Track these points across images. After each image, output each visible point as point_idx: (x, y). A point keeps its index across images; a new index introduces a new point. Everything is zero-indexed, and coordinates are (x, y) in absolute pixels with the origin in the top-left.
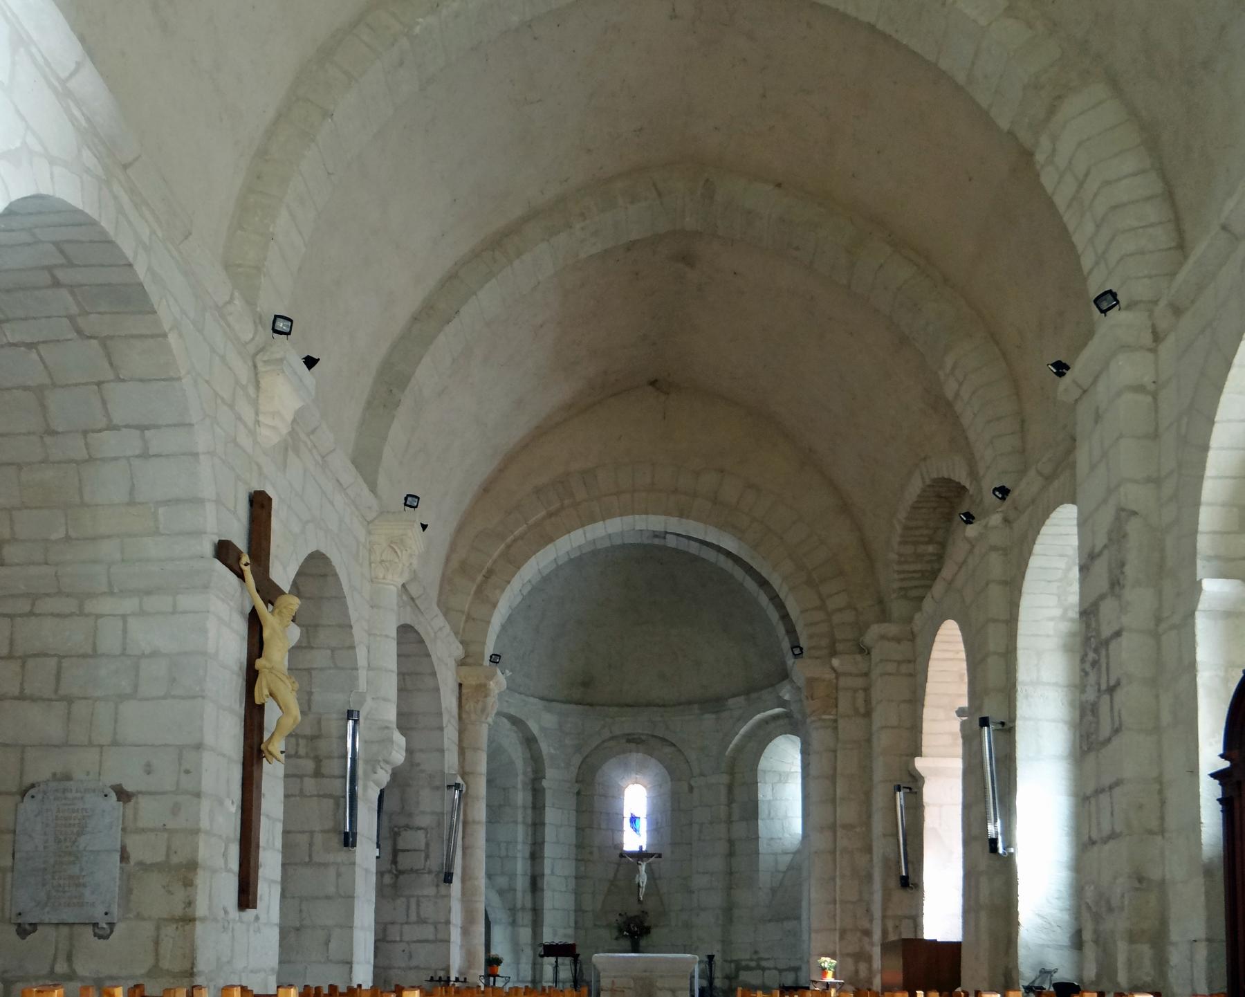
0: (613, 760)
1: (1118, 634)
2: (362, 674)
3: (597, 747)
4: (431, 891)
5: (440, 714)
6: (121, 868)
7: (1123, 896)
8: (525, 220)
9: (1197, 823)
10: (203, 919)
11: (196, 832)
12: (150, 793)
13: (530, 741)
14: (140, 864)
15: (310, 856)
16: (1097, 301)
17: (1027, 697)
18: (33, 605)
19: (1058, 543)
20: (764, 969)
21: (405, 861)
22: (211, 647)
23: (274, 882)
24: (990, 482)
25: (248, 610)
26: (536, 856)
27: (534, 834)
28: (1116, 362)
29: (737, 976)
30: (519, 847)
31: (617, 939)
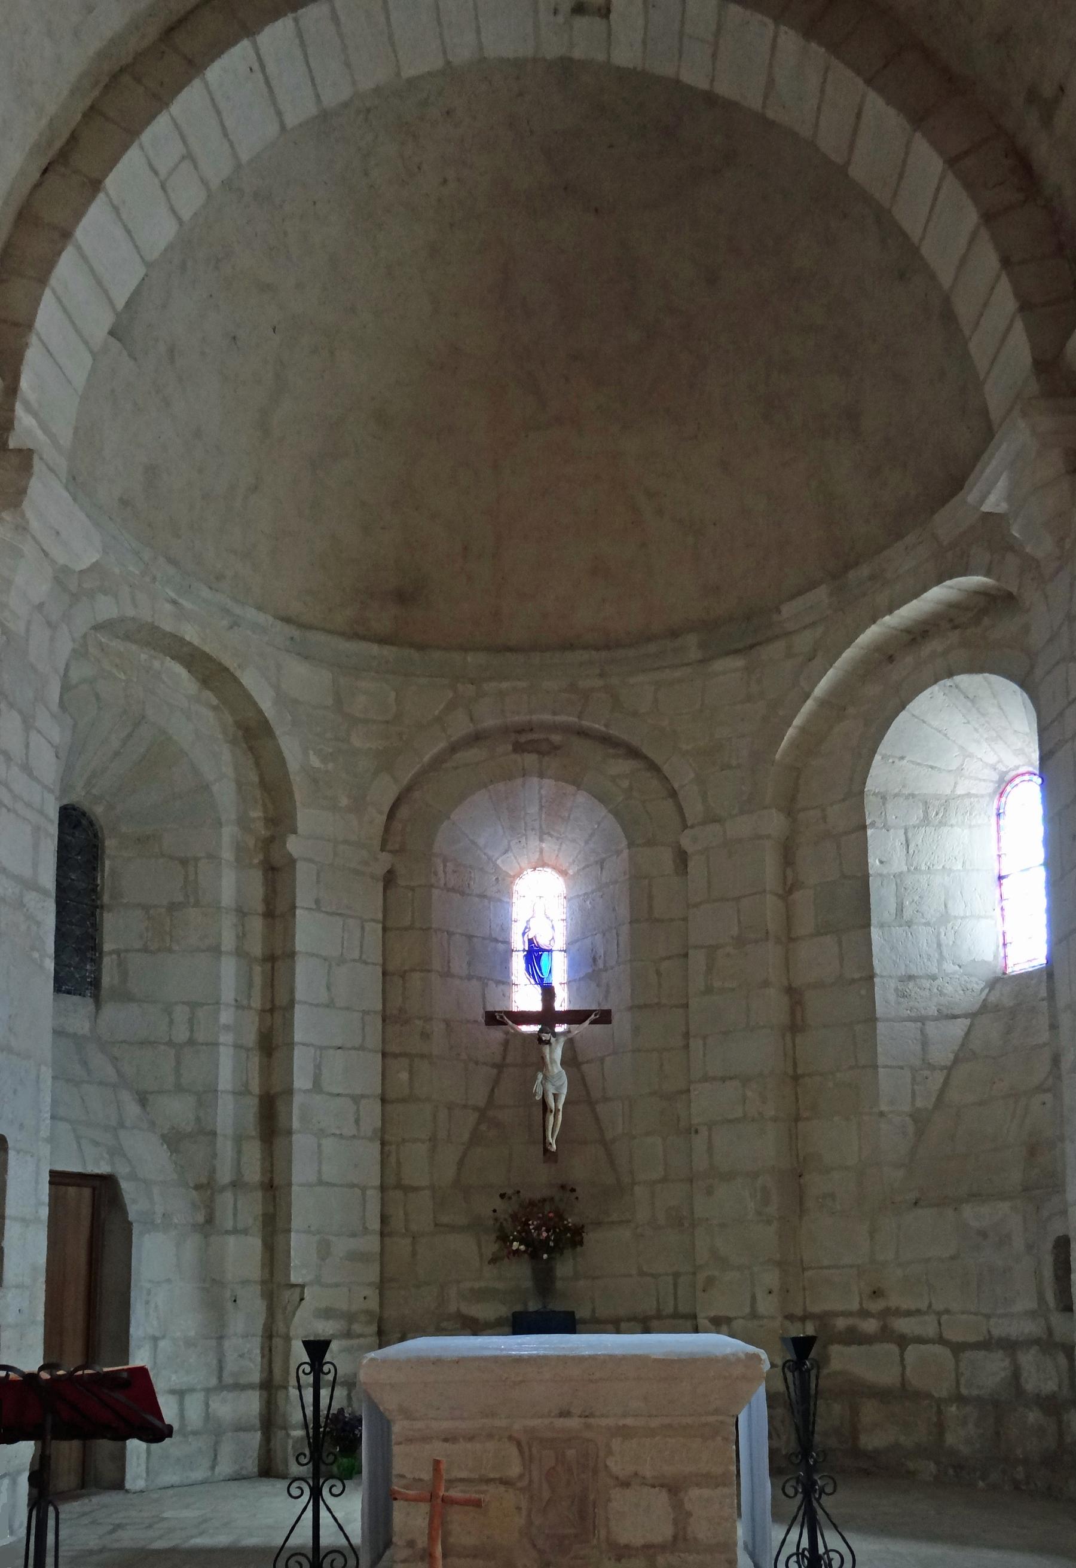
0: (481, 797)
3: (437, 762)
13: (253, 734)
20: (903, 1341)
30: (226, 1017)
31: (494, 1260)
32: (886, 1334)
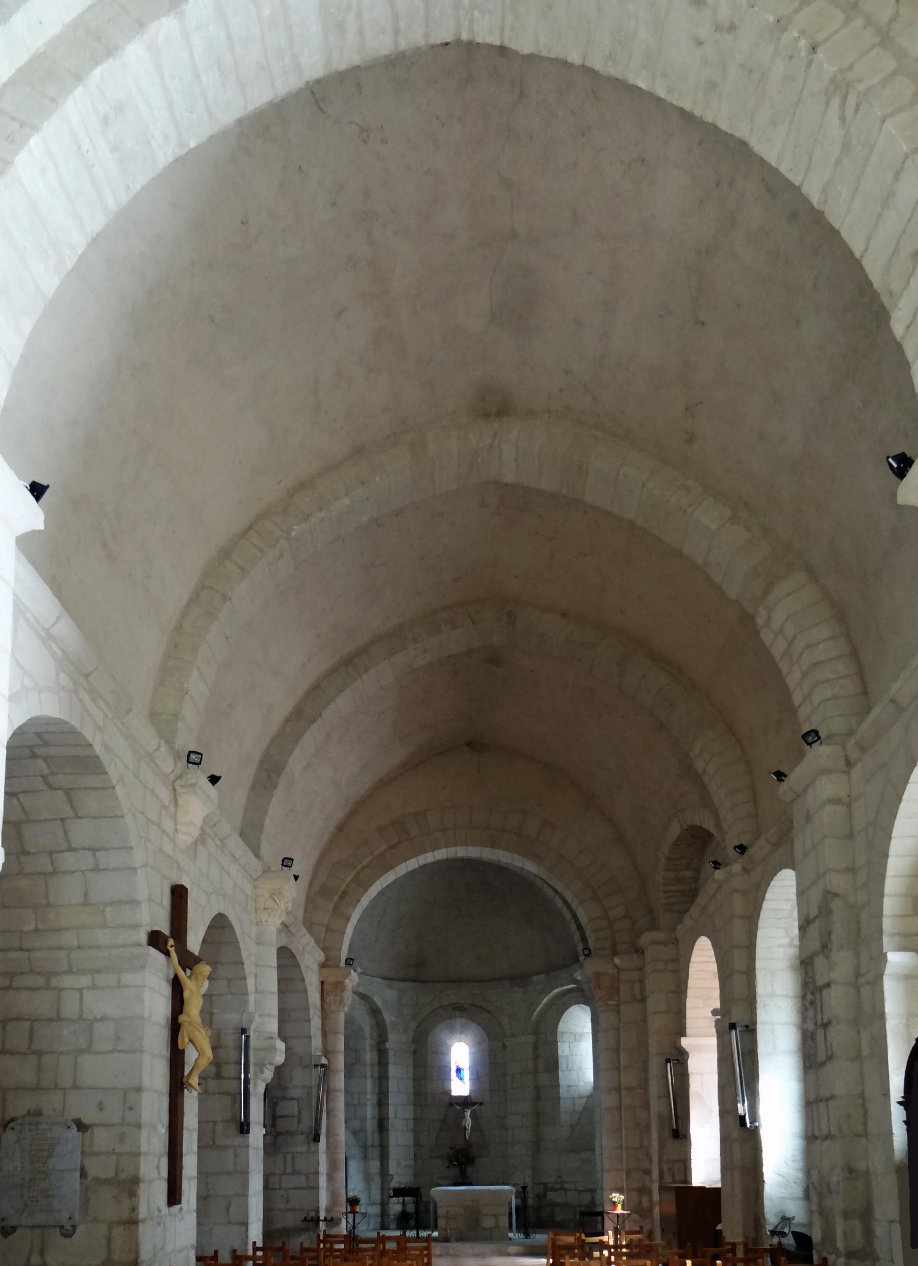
1: (828, 985)
2: (252, 998)
4: (303, 1148)
5: (308, 1009)
6: (81, 1184)
7: (838, 1183)
8: (372, 643)
9: (890, 1133)
10: (144, 1220)
11: (138, 1155)
12: (102, 1125)
13: (375, 1012)
14: (96, 1180)
15: (213, 1141)
16: (804, 737)
17: (764, 1006)
18: (11, 981)
19: (782, 897)
20: (566, 1190)
21: (282, 1125)
22: (146, 1015)
23: (193, 1178)
24: (732, 840)
25: (172, 976)
26: (382, 1103)
27: (380, 1085)
28: (819, 781)
29: (545, 1195)
30: (369, 1096)
32: (562, 1188)
